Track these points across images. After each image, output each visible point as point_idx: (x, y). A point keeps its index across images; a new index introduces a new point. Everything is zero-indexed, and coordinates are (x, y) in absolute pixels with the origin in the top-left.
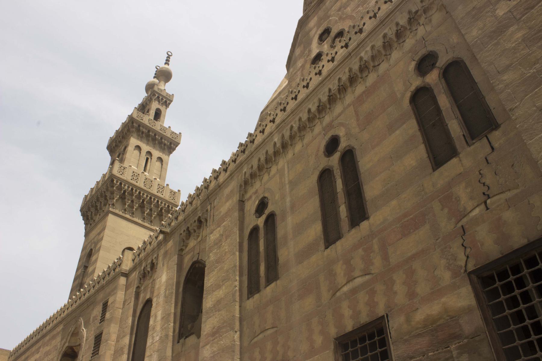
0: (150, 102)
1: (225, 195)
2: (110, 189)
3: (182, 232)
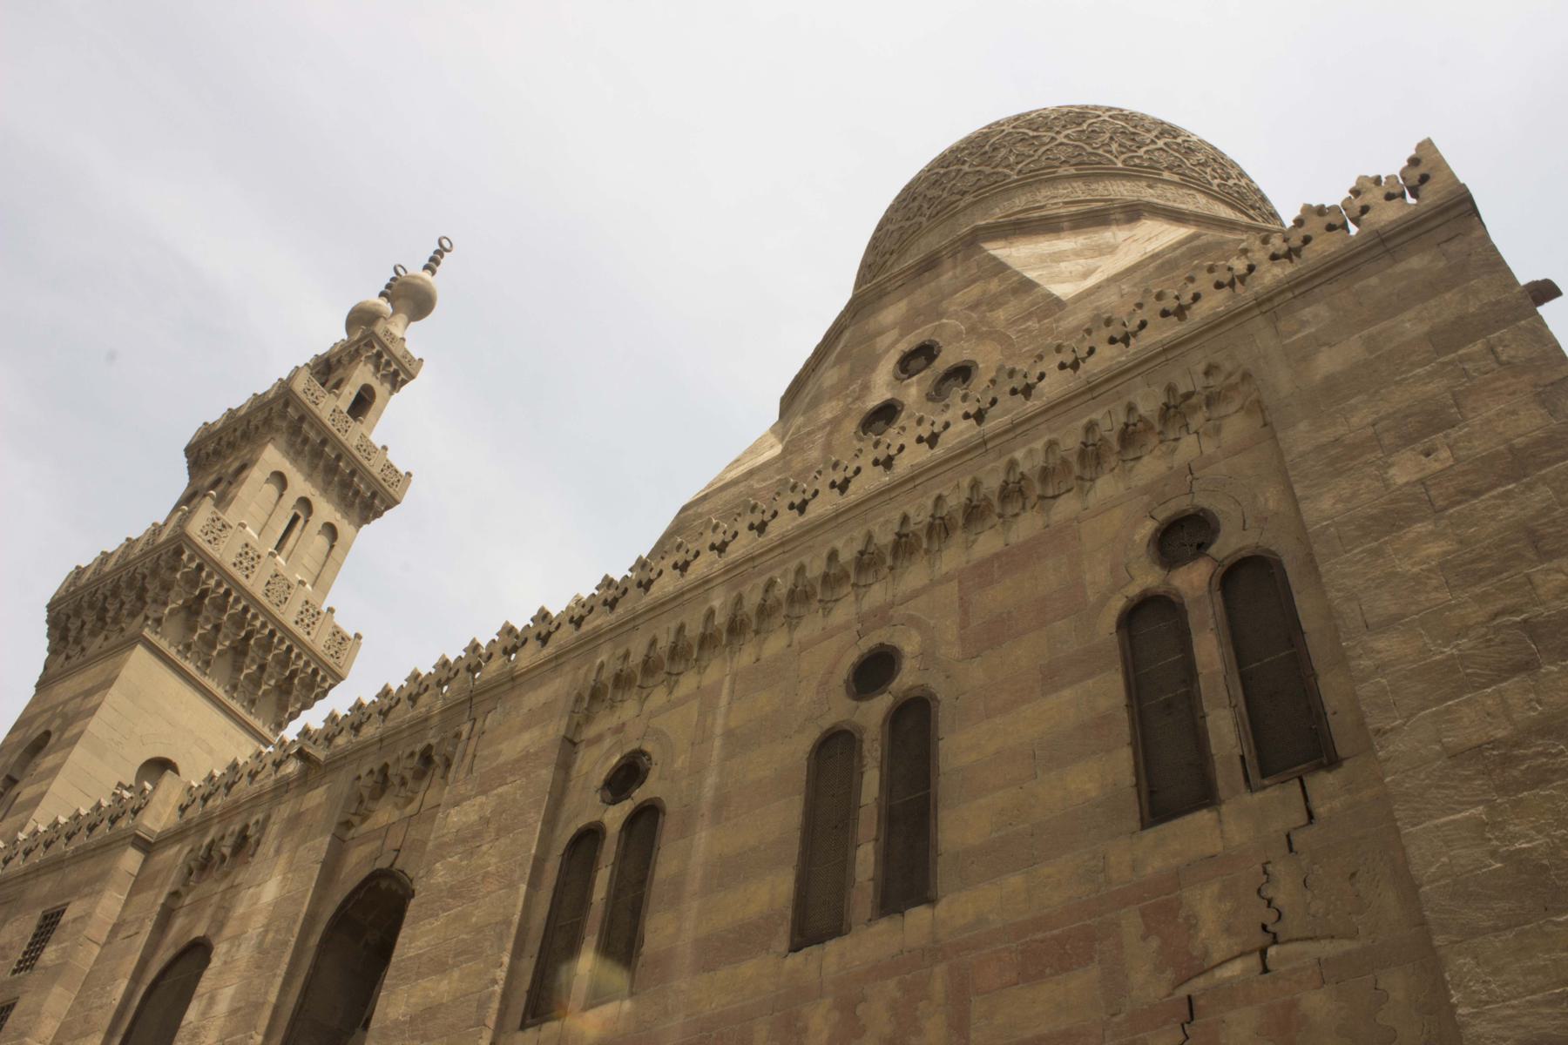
1: (525, 710)
3: (364, 772)
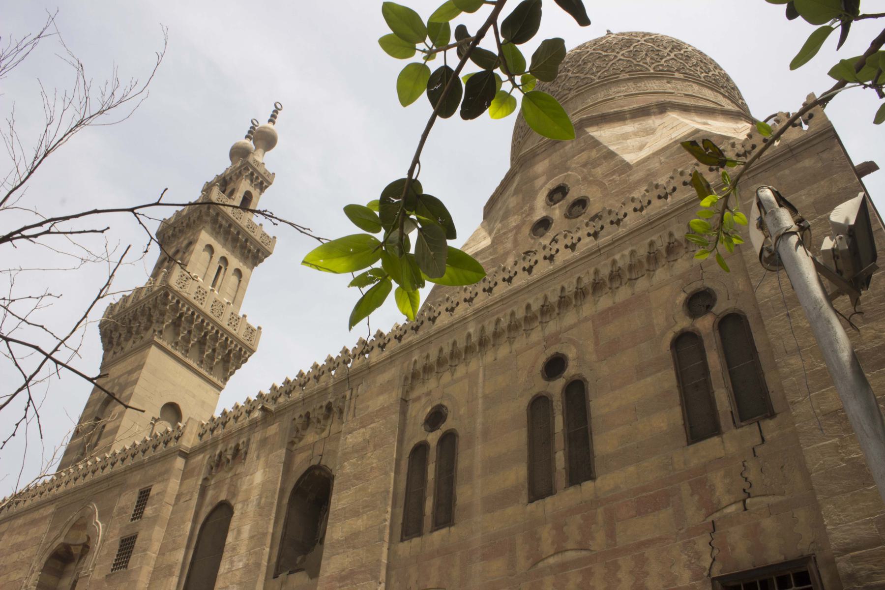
0: (237, 179)
2: (160, 306)
3: (297, 416)
